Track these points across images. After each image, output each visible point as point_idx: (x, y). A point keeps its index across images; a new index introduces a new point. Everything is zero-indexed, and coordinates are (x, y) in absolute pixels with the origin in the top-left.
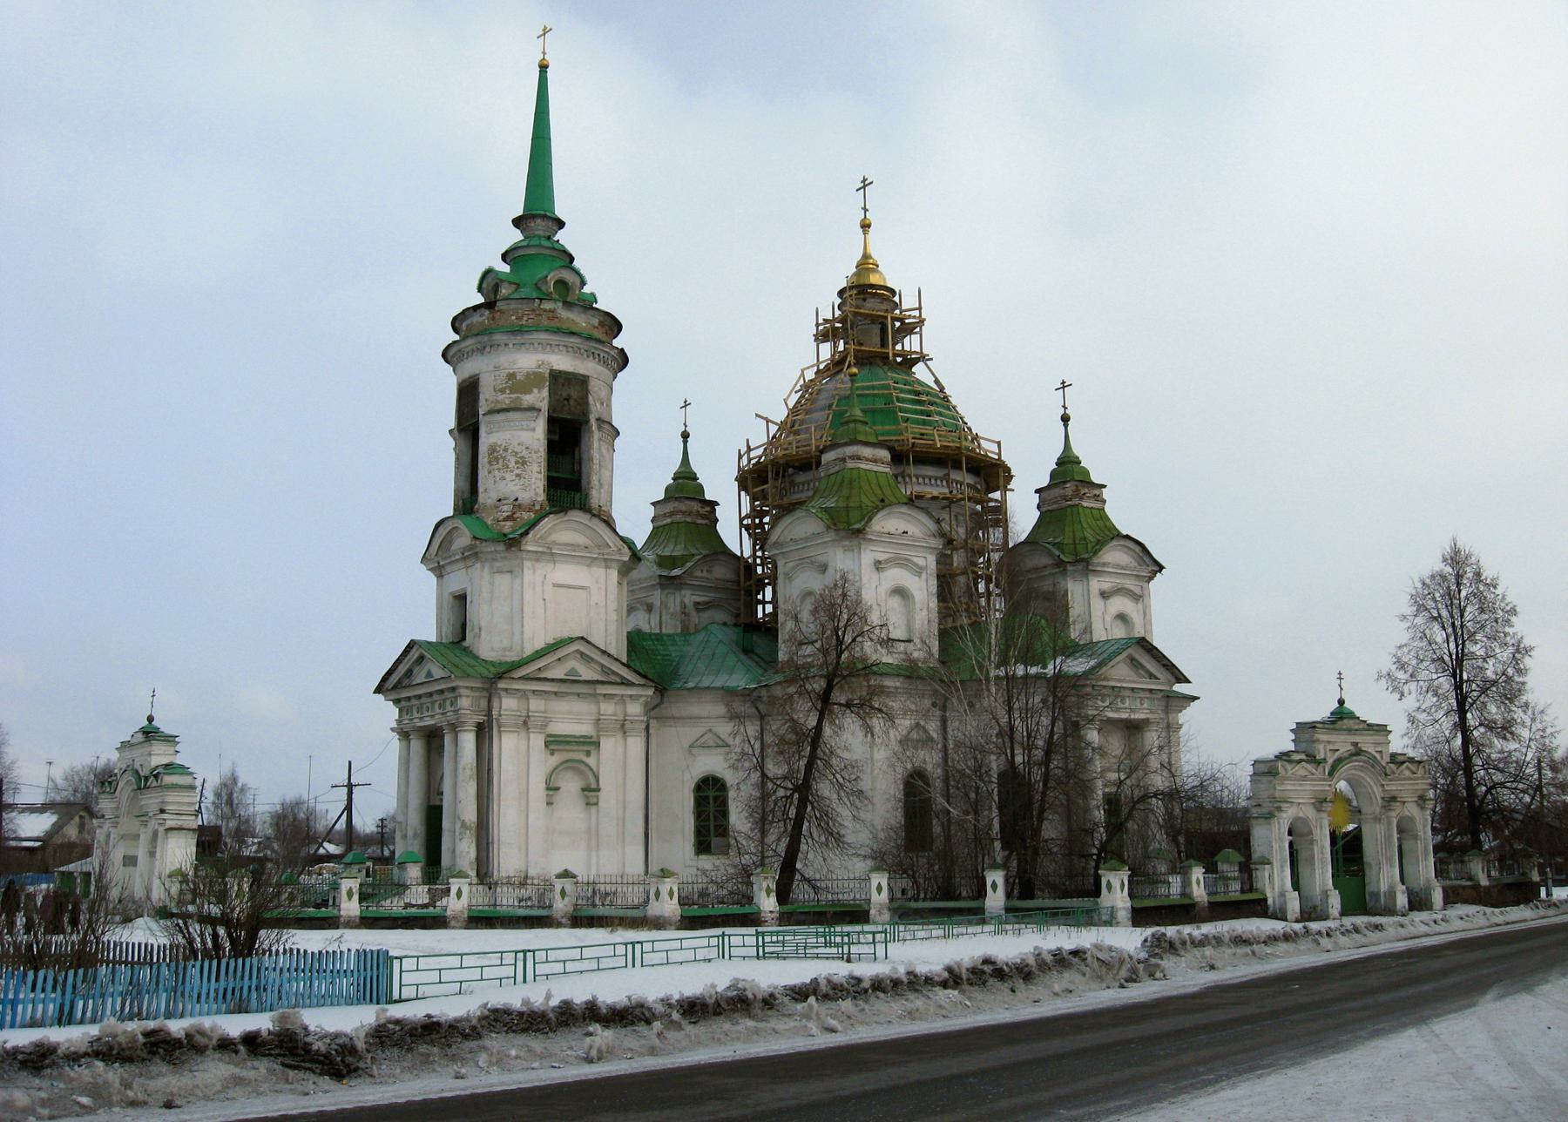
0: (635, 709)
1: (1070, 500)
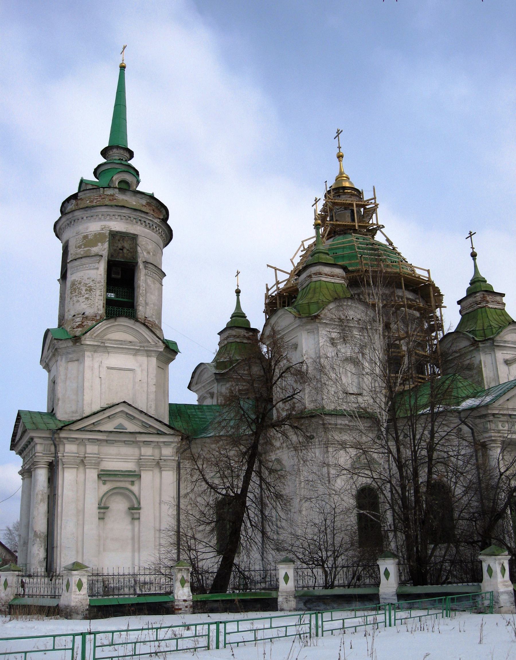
0: (168, 452)
1: (480, 303)
